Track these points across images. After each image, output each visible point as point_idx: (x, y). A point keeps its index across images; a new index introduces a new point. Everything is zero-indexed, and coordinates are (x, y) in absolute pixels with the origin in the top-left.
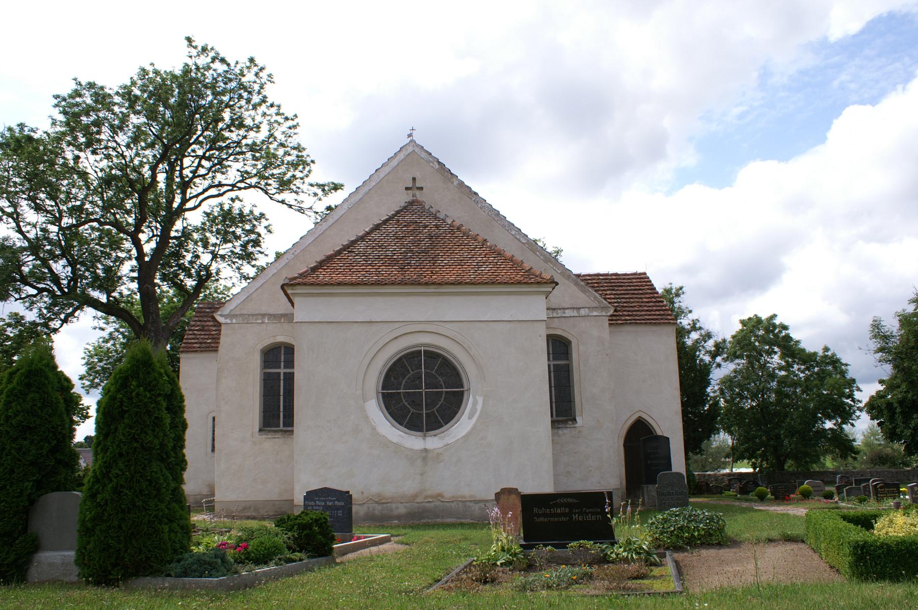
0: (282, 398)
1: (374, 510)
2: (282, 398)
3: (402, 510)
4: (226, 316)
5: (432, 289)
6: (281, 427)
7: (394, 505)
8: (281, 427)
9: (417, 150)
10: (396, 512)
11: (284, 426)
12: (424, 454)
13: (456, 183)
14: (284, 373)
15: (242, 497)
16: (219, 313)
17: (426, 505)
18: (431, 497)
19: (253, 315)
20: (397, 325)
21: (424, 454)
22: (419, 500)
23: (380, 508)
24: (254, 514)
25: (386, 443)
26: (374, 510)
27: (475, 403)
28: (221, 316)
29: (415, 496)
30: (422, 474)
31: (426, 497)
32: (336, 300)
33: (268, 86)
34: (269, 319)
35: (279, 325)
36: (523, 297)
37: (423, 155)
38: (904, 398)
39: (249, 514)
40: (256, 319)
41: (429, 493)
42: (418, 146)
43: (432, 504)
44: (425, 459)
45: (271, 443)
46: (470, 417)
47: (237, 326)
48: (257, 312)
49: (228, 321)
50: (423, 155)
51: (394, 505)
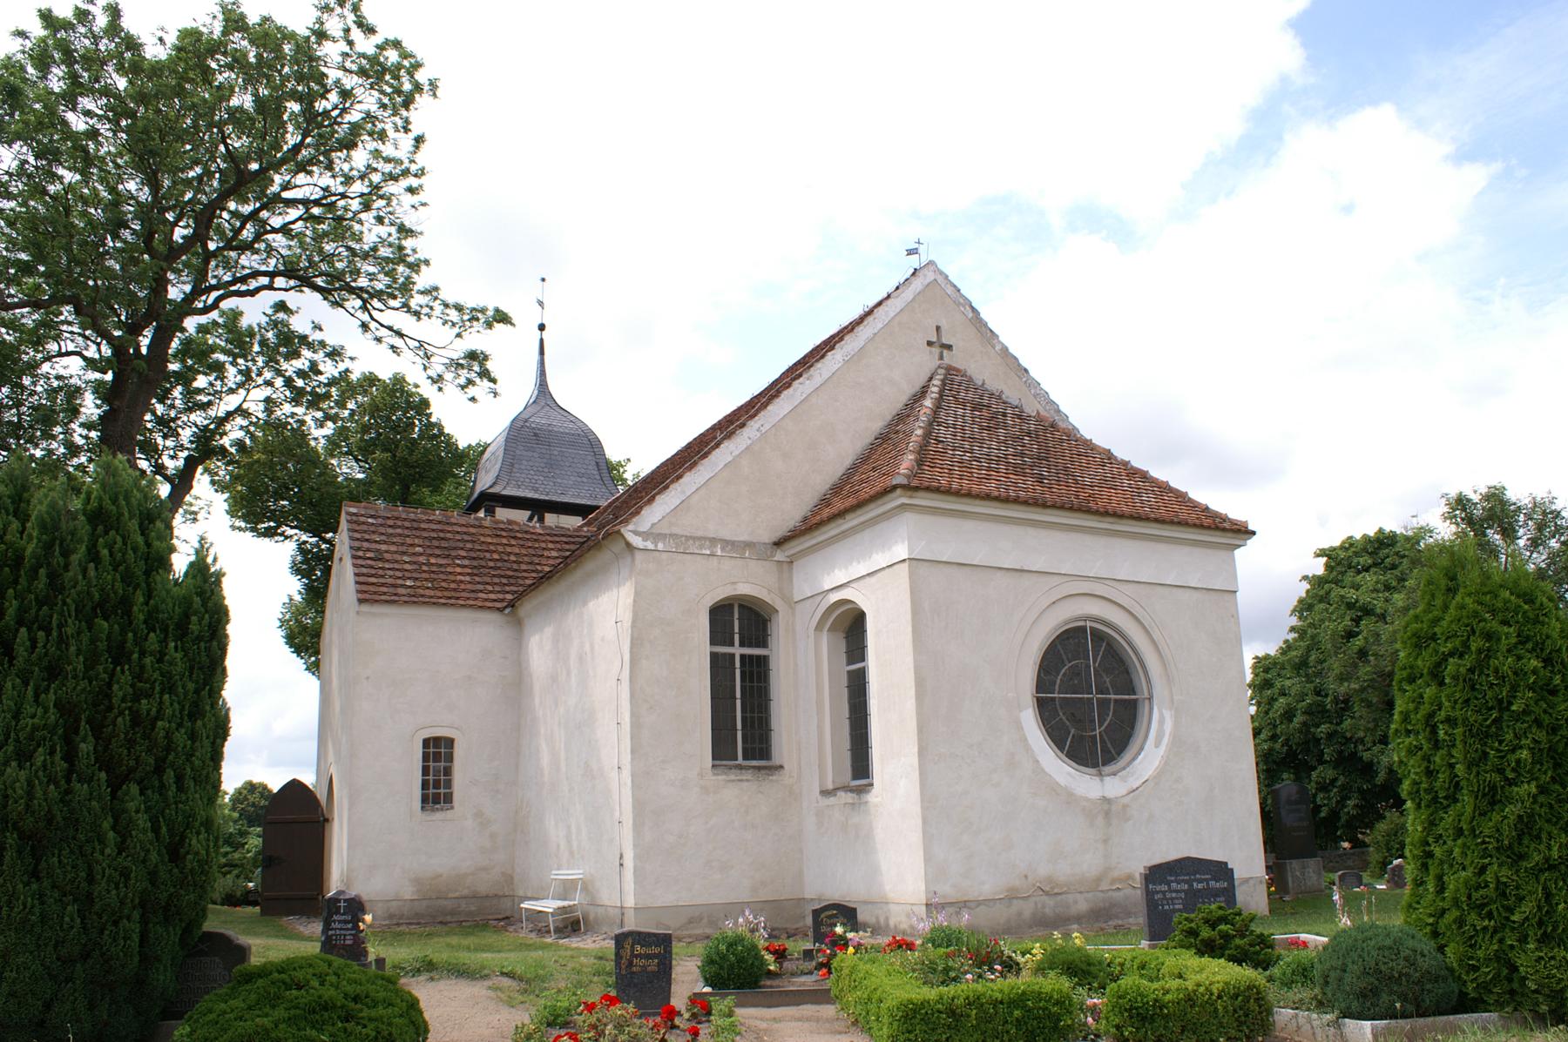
0: (738, 703)
1: (1044, 907)
2: (738, 703)
3: (1081, 905)
4: (645, 535)
5: (1105, 524)
6: (740, 760)
7: (1070, 898)
8: (740, 760)
9: (940, 280)
10: (1074, 910)
11: (745, 758)
12: (1106, 807)
13: (998, 348)
14: (743, 657)
15: (685, 899)
16: (631, 527)
17: (1115, 894)
18: (1120, 880)
19: (694, 539)
20: (1057, 580)
21: (1106, 807)
22: (1104, 886)
23: (1050, 902)
24: (708, 931)
25: (1054, 789)
26: (1044, 907)
27: (1162, 722)
28: (636, 533)
29: (1099, 880)
30: (1105, 841)
31: (1113, 881)
32: (969, 525)
33: (422, 100)
34: (723, 549)
35: (740, 562)
36: (1209, 551)
37: (950, 290)
38: (1271, 749)
39: (699, 932)
40: (701, 547)
41: (1116, 874)
42: (941, 273)
43: (1121, 894)
44: (1107, 814)
45: (737, 792)
46: (1157, 745)
47: (665, 555)
48: (700, 534)
49: (650, 545)
50: (950, 290)
51: (1070, 898)
